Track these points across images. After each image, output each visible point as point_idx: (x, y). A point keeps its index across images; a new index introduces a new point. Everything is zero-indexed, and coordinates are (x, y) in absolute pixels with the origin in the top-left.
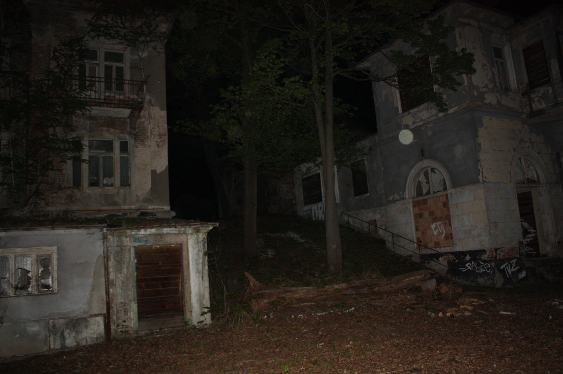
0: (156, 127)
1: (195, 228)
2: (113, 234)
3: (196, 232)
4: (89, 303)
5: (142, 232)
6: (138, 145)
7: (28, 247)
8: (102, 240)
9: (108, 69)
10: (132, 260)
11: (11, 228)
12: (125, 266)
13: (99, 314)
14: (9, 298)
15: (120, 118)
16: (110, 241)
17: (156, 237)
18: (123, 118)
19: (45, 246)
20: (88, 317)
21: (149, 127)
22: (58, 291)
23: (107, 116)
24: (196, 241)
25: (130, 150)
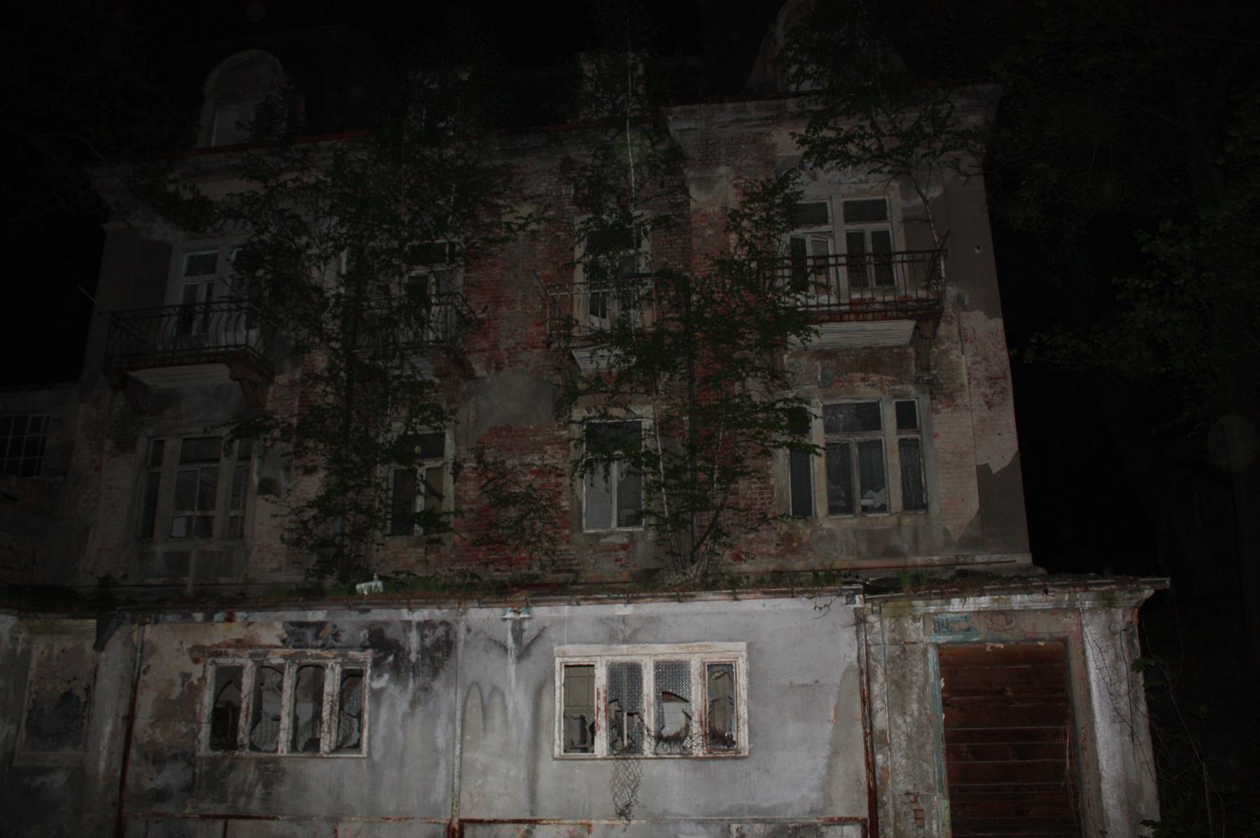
0: (979, 359)
1: (1103, 592)
2: (881, 610)
3: (1104, 606)
4: (826, 786)
5: (956, 605)
6: (939, 406)
7: (682, 642)
8: (854, 628)
9: (854, 240)
10: (932, 679)
11: (641, 595)
12: (915, 697)
13: (850, 819)
14: (642, 761)
15: (891, 348)
16: (875, 630)
17: (994, 620)
18: (899, 347)
19: (718, 640)
20: (823, 825)
21: (964, 361)
22: (749, 752)
23: (860, 347)
24: (1107, 631)
25: (920, 417)
